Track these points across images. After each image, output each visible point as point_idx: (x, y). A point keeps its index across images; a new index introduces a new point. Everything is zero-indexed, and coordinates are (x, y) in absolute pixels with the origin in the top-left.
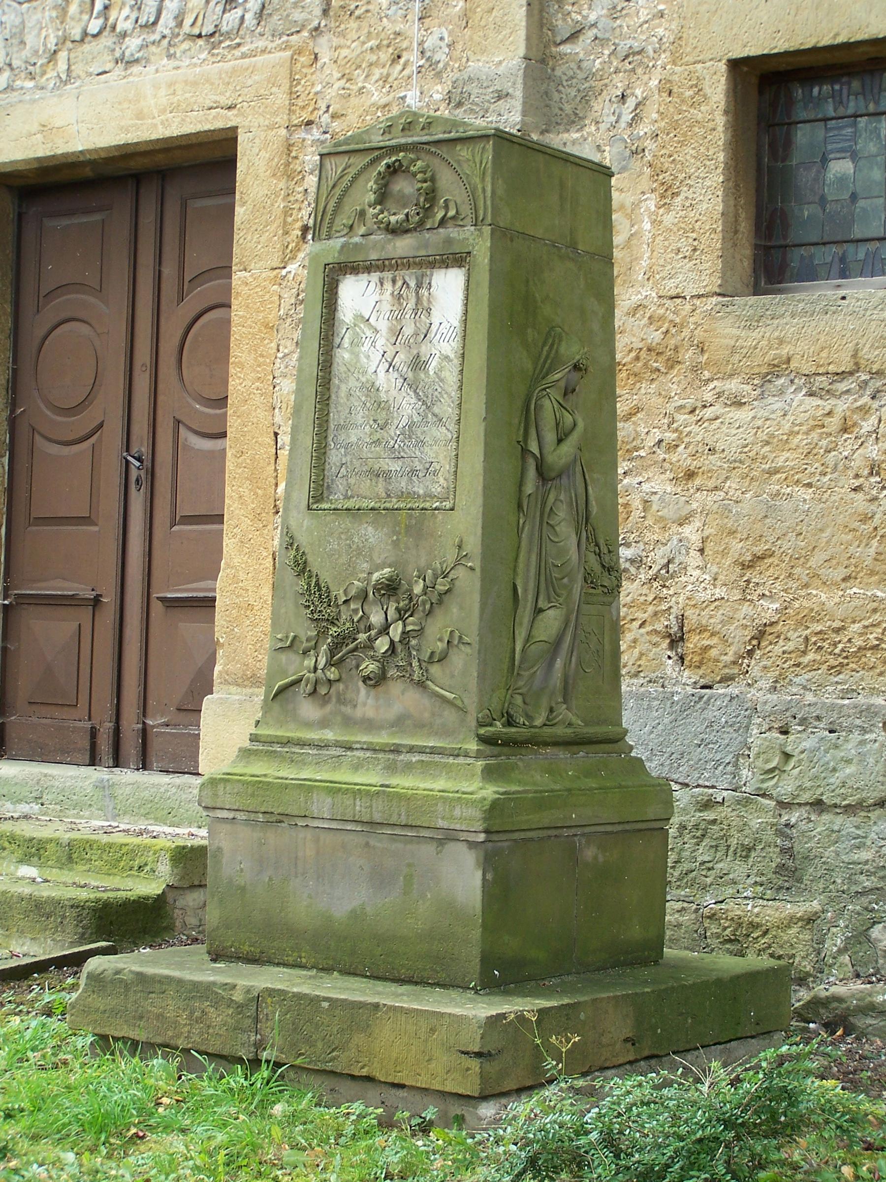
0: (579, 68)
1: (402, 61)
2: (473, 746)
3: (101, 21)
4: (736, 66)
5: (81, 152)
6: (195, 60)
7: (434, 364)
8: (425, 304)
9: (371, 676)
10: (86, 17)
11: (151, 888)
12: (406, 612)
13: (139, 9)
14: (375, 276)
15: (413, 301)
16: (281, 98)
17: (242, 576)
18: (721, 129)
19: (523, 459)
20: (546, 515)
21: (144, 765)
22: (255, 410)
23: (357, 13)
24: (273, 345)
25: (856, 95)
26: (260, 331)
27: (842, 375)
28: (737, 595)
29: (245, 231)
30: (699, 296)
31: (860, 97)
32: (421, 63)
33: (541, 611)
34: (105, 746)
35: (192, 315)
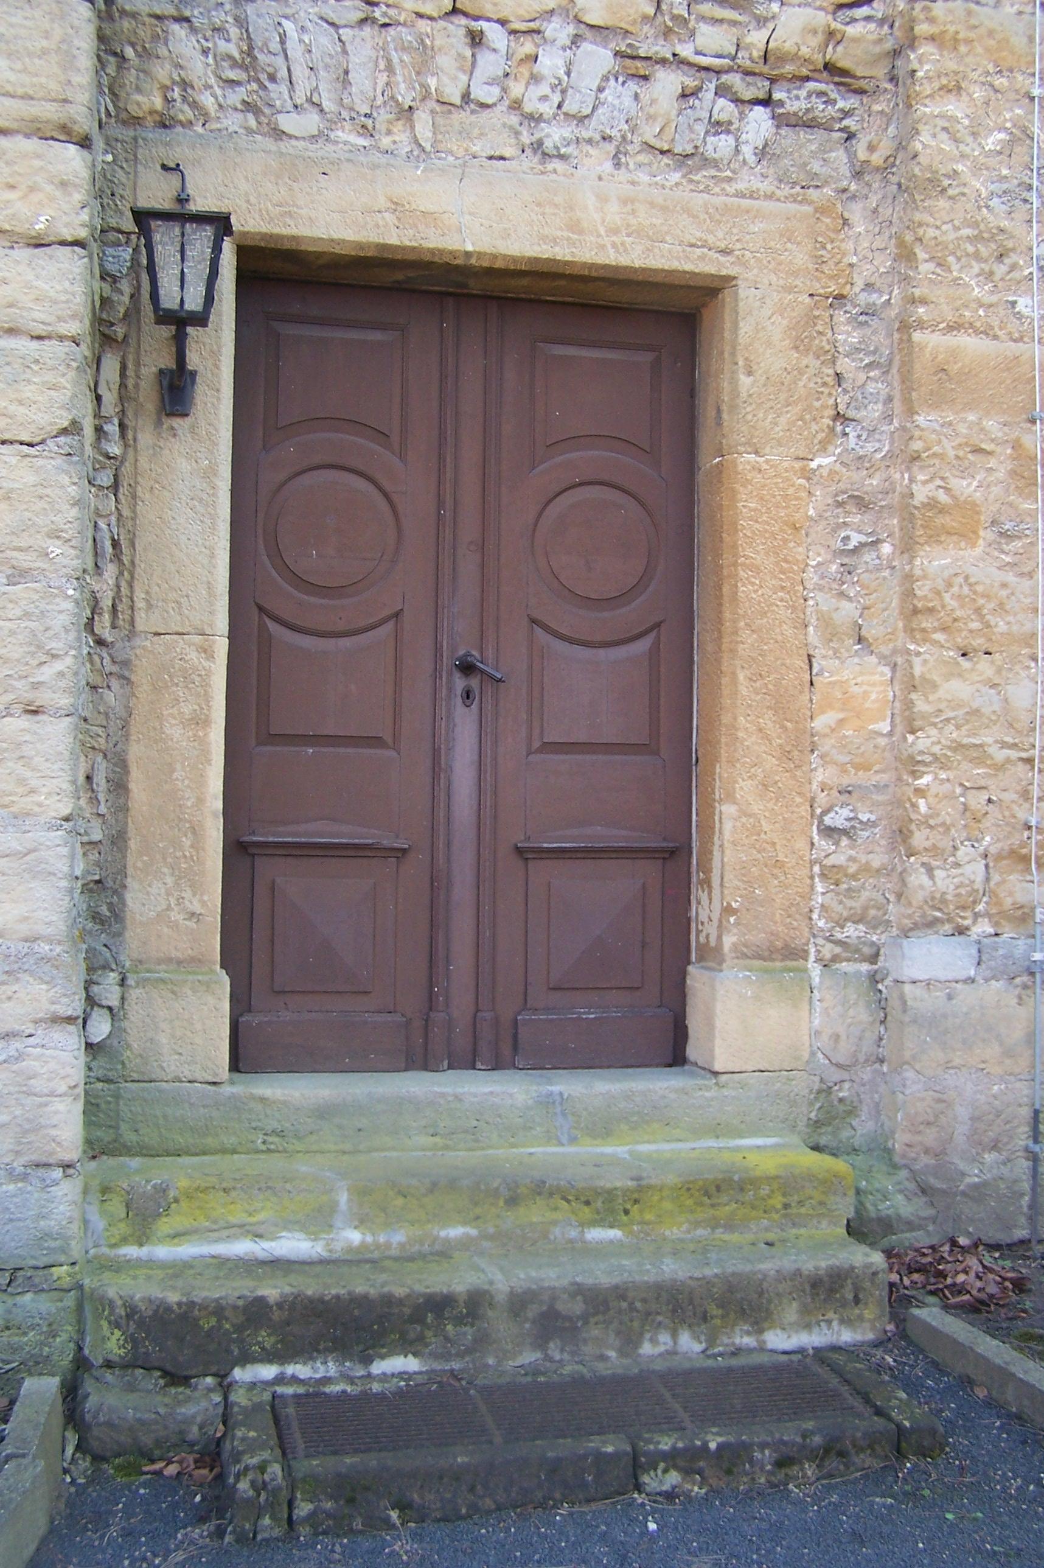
13: (563, 92)
17: (766, 826)
22: (780, 626)
23: (950, 192)
26: (781, 530)
29: (754, 406)
34: (506, 1050)
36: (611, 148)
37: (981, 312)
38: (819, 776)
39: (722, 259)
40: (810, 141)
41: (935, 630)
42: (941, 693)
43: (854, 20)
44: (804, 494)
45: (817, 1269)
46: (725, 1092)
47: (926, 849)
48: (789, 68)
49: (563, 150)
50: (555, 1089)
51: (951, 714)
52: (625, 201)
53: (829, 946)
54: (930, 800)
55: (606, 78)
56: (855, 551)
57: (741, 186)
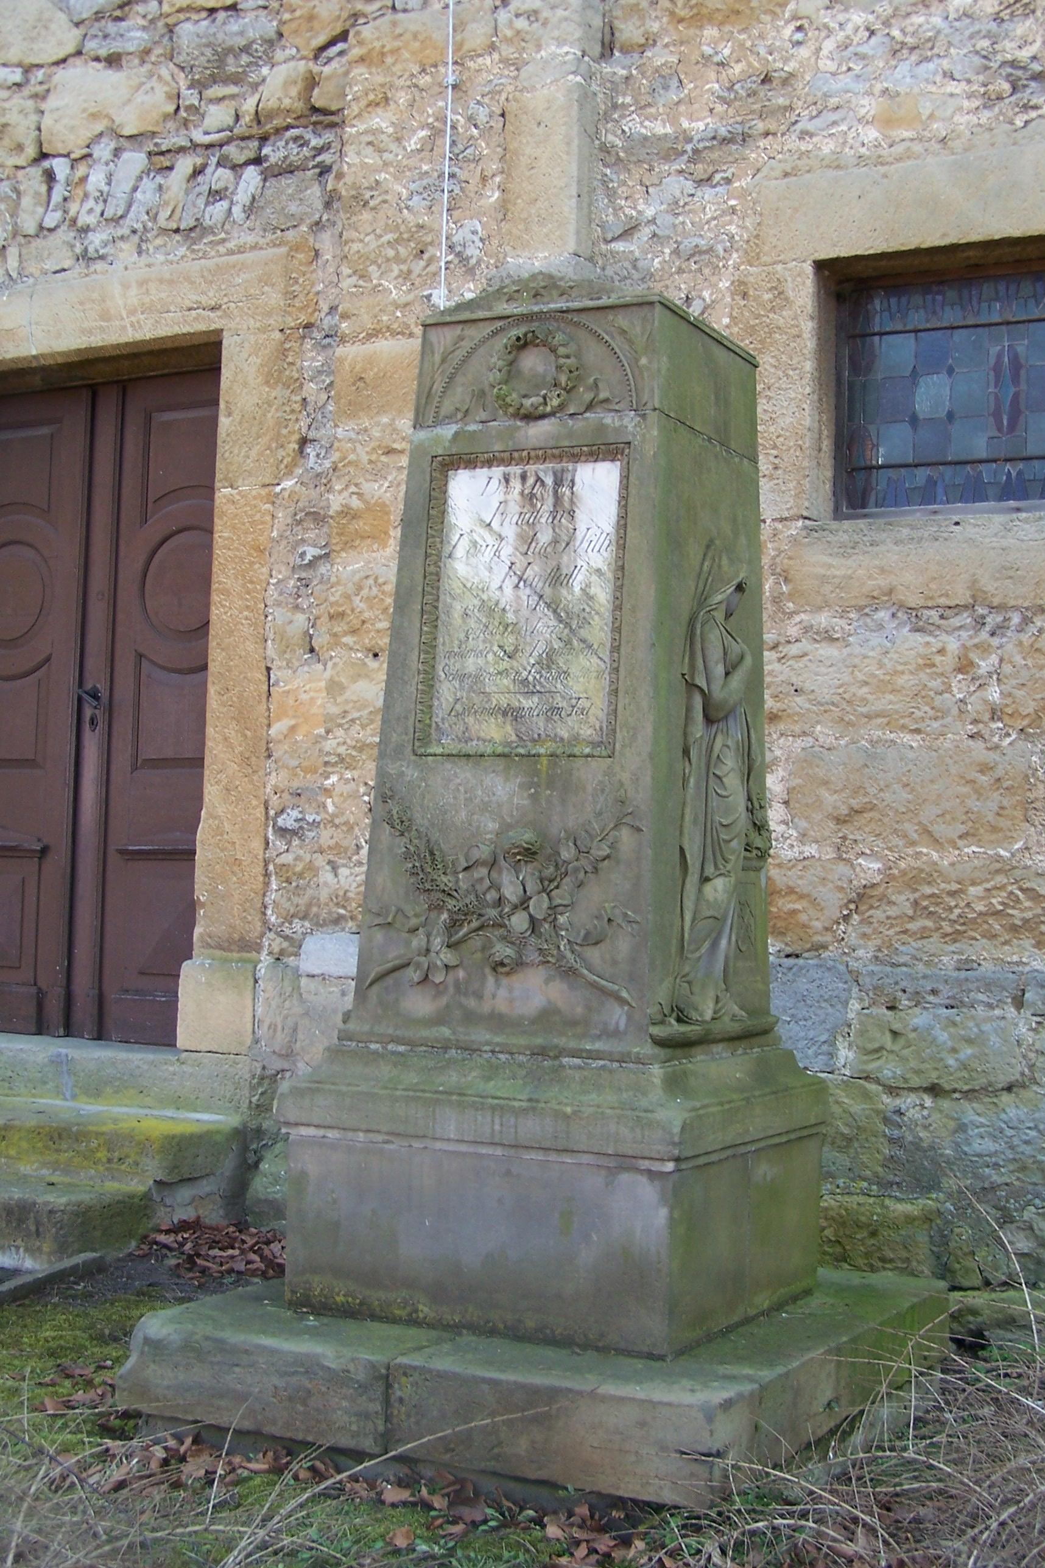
0: (635, 267)
1: (426, 256)
2: (647, 1049)
3: (58, 215)
4: (821, 266)
5: (34, 357)
6: (171, 257)
7: (580, 577)
8: (567, 505)
9: (506, 961)
10: (40, 210)
11: (137, 1186)
12: (551, 881)
13: (105, 201)
14: (498, 472)
15: (550, 501)
16: (274, 297)
17: (227, 826)
18: (806, 335)
19: (689, 698)
20: (711, 760)
21: (100, 1035)
24: (265, 570)
25: (952, 305)
26: (249, 554)
27: (958, 608)
28: (830, 854)
30: (782, 520)
31: (957, 308)
32: (450, 258)
33: (707, 880)
35: (158, 538)
36: (135, 239)
37: (399, 314)
38: (273, 780)
39: (211, 314)
40: (288, 183)
41: (345, 634)
42: (348, 694)
43: (330, 60)
44: (268, 518)
45: (11, 1199)
46: (184, 1067)
47: (329, 847)
48: (277, 122)
49: (101, 252)
50: (63, 1051)
51: (356, 715)
52: (142, 283)
53: (279, 940)
54: (336, 799)
55: (140, 178)
56: (312, 564)
57: (230, 245)
